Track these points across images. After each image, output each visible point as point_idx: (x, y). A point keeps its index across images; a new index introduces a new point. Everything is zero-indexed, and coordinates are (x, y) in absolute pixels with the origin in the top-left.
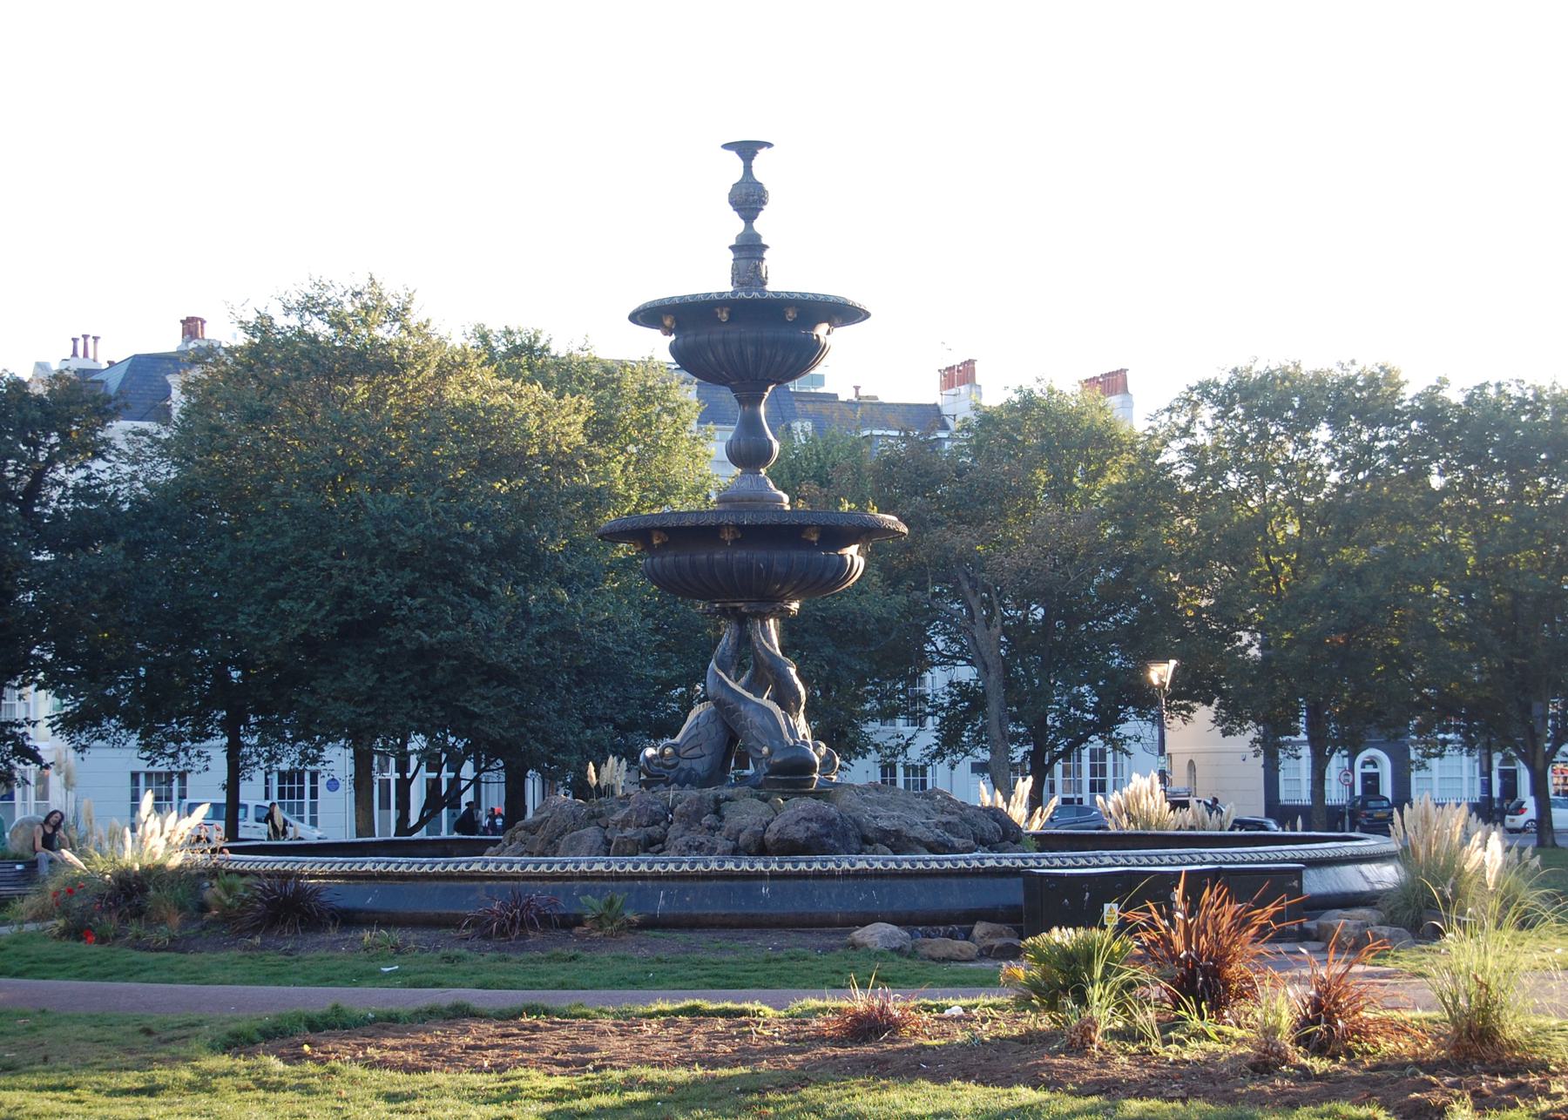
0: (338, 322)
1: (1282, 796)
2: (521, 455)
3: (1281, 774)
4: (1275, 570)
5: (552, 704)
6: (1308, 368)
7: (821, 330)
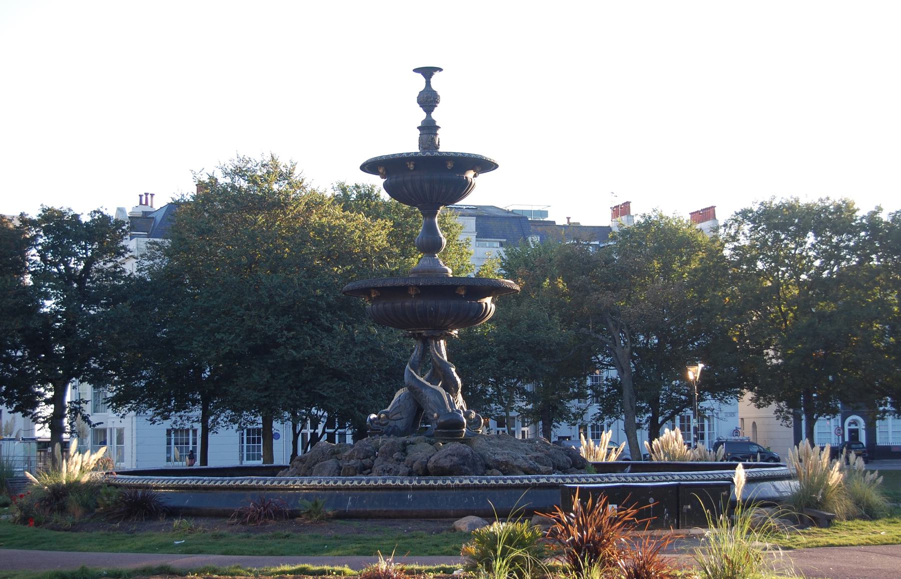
0: (253, 181)
1: (878, 441)
2: (350, 253)
3: (877, 429)
4: (785, 315)
5: (371, 391)
6: (803, 202)
7: (470, 174)
